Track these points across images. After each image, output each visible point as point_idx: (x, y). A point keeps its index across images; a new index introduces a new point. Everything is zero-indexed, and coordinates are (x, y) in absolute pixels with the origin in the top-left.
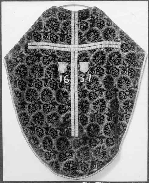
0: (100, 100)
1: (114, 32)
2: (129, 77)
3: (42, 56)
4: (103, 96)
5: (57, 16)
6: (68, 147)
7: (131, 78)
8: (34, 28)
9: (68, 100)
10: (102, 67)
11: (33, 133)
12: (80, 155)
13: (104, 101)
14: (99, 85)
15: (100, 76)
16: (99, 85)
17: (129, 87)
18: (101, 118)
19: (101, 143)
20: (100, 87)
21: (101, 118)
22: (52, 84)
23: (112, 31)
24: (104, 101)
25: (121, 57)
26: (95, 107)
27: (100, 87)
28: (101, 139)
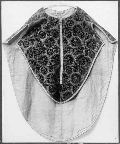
0: (69, 55)
1: (76, 25)
2: (67, 73)
3: (72, 85)
4: (83, 53)
5: (72, 90)
6: (80, 81)
7: (68, 74)
8: (66, 63)
9: (52, 25)
10: (70, 66)
11: (50, 35)
12: (78, 61)
13: (41, 11)
14: (68, 44)
15: (68, 37)
16: (68, 44)
17: (54, 45)
18: (69, 33)
19: (69, 52)
20: (68, 45)
21: (69, 33)
22: (68, 69)
23: (75, 27)
24: (41, 11)
25: (95, 45)
26: (52, 60)
27: (68, 45)
28: (69, 49)
